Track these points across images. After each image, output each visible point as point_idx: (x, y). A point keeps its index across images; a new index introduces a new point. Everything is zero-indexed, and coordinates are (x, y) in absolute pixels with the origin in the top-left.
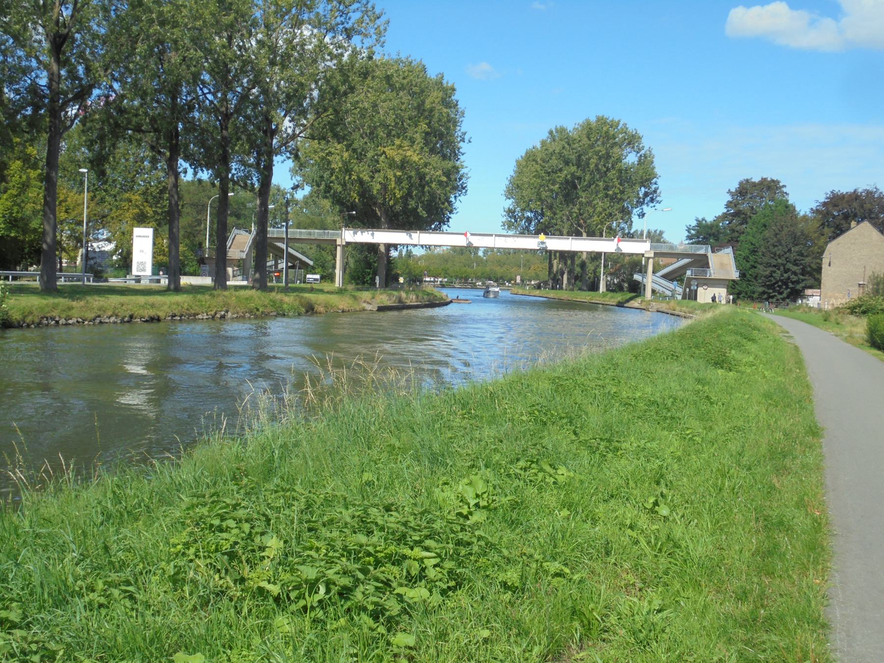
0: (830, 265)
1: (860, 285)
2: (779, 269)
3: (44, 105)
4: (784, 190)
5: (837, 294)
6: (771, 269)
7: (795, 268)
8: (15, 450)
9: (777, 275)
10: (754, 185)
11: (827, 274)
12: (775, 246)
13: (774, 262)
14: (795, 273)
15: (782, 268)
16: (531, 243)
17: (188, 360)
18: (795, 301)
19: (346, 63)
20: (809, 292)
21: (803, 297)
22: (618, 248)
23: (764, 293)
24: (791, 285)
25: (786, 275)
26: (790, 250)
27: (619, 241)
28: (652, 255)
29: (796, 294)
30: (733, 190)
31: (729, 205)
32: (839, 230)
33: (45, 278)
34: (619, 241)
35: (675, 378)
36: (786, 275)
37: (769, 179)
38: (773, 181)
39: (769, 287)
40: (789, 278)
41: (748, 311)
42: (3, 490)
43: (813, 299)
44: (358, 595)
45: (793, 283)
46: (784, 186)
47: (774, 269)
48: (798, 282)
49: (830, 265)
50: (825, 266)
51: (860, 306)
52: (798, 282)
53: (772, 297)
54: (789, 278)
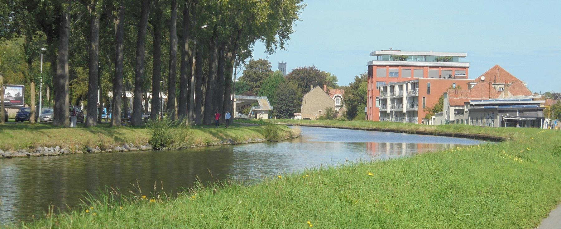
1: (319, 111)
2: (284, 105)
3: (123, 114)
4: (270, 65)
5: (308, 115)
6: (281, 105)
9: (284, 108)
11: (304, 107)
12: (282, 96)
13: (282, 102)
14: (291, 107)
15: (286, 105)
17: (372, 78)
18: (290, 118)
19: (50, 54)
20: (295, 114)
24: (289, 112)
25: (287, 108)
26: (288, 97)
29: (292, 115)
32: (306, 89)
35: (422, 177)
36: (287, 108)
37: (263, 60)
40: (288, 109)
41: (274, 120)
42: (195, 98)
43: (299, 117)
44: (196, 214)
45: (290, 111)
46: (270, 63)
47: (282, 105)
51: (340, 119)
53: (281, 117)
54: (288, 109)
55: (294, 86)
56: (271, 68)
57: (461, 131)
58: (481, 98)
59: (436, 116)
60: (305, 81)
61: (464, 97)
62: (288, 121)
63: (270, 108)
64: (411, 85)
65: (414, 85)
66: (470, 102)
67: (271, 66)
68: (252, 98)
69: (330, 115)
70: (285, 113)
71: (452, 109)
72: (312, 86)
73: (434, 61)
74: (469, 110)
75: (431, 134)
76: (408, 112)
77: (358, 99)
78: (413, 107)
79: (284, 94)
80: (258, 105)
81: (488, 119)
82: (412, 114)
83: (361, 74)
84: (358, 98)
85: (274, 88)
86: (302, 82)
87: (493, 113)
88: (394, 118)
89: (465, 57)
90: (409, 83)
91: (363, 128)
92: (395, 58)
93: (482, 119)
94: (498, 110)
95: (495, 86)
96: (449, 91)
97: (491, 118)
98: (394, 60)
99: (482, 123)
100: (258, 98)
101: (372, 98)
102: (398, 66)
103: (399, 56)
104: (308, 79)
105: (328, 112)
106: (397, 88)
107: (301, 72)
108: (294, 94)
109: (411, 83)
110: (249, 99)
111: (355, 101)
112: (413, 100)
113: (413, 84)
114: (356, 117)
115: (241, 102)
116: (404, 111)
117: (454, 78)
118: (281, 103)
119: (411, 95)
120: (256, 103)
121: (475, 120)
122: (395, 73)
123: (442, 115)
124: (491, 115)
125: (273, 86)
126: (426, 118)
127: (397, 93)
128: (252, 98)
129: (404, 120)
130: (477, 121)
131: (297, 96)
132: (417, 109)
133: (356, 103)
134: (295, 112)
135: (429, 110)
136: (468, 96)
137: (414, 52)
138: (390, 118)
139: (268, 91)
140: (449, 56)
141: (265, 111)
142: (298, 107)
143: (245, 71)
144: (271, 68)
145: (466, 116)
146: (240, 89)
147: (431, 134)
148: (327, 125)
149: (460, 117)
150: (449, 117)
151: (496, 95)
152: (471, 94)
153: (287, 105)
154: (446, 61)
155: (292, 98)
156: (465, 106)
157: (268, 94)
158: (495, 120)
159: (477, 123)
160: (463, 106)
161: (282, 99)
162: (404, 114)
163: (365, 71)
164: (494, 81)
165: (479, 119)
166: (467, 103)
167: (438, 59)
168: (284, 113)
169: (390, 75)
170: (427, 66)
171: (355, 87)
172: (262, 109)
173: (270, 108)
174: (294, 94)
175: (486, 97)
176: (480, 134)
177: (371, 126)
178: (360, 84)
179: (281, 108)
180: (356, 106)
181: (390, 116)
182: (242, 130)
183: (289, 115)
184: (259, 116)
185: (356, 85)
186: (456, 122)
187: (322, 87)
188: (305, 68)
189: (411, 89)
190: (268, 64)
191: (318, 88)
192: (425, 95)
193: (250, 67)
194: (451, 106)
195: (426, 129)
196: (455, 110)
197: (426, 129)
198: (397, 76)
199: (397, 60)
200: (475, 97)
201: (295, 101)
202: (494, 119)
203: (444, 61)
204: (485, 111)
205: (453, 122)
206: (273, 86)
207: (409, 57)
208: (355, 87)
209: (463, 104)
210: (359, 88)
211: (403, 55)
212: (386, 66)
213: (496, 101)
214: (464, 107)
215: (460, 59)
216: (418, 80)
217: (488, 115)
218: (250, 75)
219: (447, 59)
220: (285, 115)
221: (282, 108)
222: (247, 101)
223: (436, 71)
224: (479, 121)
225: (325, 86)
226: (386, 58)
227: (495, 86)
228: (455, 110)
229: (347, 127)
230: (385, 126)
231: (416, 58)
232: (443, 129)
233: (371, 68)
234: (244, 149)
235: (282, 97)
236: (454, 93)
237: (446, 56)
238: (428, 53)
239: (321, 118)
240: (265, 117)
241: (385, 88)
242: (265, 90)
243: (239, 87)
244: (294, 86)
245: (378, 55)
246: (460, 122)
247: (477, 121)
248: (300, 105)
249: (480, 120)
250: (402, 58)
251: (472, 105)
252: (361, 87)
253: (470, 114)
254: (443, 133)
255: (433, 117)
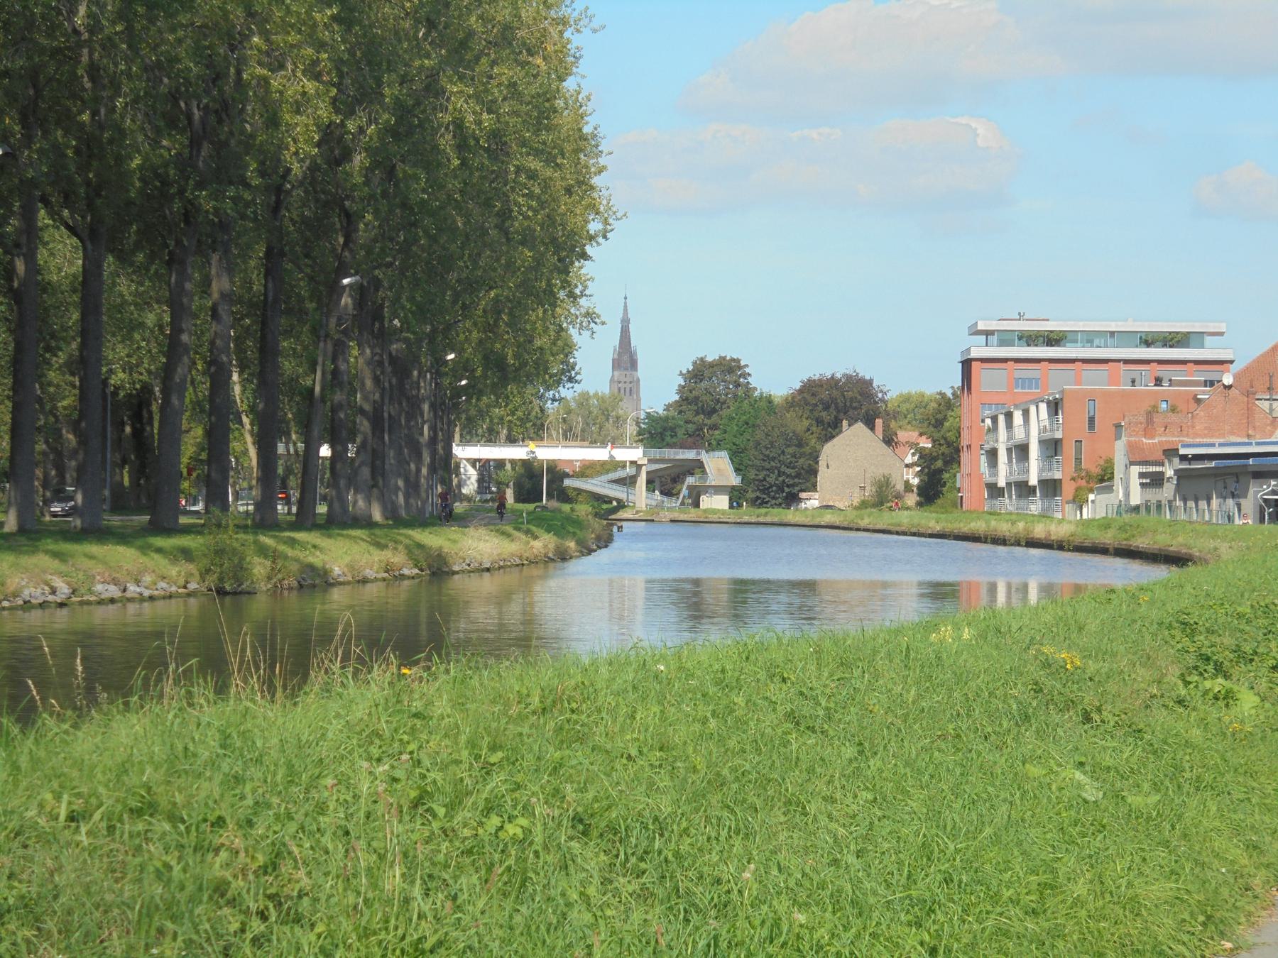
0: (828, 467)
2: (773, 473)
4: (747, 370)
7: (789, 471)
8: (29, 687)
9: (772, 479)
10: (712, 365)
12: (767, 448)
13: (766, 465)
14: (789, 476)
16: (546, 453)
20: (803, 495)
21: (800, 500)
22: (611, 456)
23: (758, 498)
24: (787, 490)
25: (781, 479)
27: (612, 448)
28: (646, 462)
29: (792, 499)
30: (684, 371)
31: (681, 389)
32: (830, 430)
33: (455, 481)
34: (612, 448)
36: (781, 479)
37: (728, 358)
38: (733, 360)
39: (763, 492)
43: (811, 502)
45: (788, 486)
46: (747, 366)
48: (793, 485)
49: (828, 467)
50: (822, 463)
52: (793, 485)
53: (767, 503)
55: (798, 424)
56: (750, 379)
57: (1133, 536)
58: (1224, 437)
59: (1098, 494)
60: (831, 410)
61: (1173, 435)
62: (766, 515)
63: (735, 480)
64: (1048, 407)
65: (1055, 407)
66: (1178, 450)
67: (749, 375)
68: (690, 455)
69: (883, 496)
70: (776, 492)
71: (1135, 470)
72: (845, 423)
73: (1137, 347)
74: (1176, 472)
75: (1060, 546)
76: (1043, 482)
77: (943, 454)
78: (1051, 470)
79: (771, 443)
80: (704, 472)
81: (1225, 498)
82: (1051, 487)
83: (952, 387)
84: (944, 449)
85: (750, 430)
86: (824, 414)
87: (1237, 482)
88: (1014, 501)
89: (1221, 334)
90: (1042, 401)
91: (914, 530)
92: (1030, 339)
93: (1209, 500)
94: (1250, 469)
95: (1271, 405)
96: (1127, 420)
97: (1233, 496)
98: (1029, 345)
99: (1197, 510)
100: (705, 457)
101: (969, 447)
102: (1038, 361)
103: (1042, 334)
104: (841, 405)
105: (880, 487)
106: (1018, 417)
107: (822, 386)
108: (800, 445)
109: (1049, 403)
110: (681, 457)
111: (935, 459)
112: (1052, 447)
113: (1053, 405)
114: (939, 501)
115: (662, 466)
116: (1033, 481)
117: (1170, 385)
118: (763, 468)
119: (1048, 435)
120: (698, 466)
121: (1191, 504)
122: (1030, 380)
123: (1110, 489)
124: (1232, 486)
125: (747, 424)
126: (1074, 501)
127: (1019, 434)
128: (690, 455)
129: (1033, 507)
130: (1185, 504)
131: (807, 450)
132: (1058, 476)
133: (939, 463)
134: (802, 491)
135: (1089, 477)
136: (1184, 432)
137: (1081, 323)
138: (1007, 501)
139: (735, 436)
140: (1177, 333)
141: (718, 490)
142: (808, 477)
143: (684, 387)
144: (750, 379)
145: (1168, 491)
146: (668, 433)
147: (1060, 546)
148: (846, 524)
149: (1154, 495)
150: (1127, 494)
151: (1269, 428)
152: (1193, 427)
153: (779, 472)
154: (1171, 347)
155: (794, 456)
156: (1166, 461)
157: (734, 444)
158: (1242, 501)
159: (1185, 509)
160: (1163, 465)
161: (768, 456)
162: (1032, 490)
163: (955, 379)
164: (1269, 388)
165: (1202, 500)
166: (1171, 453)
167: (1148, 341)
168: (772, 494)
169: (1017, 387)
170: (1118, 361)
171: (937, 420)
172: (713, 484)
173: (735, 480)
174: (800, 445)
175: (1238, 436)
176: (1171, 549)
177: (932, 524)
178: (950, 413)
179: (765, 479)
180: (940, 471)
181: (1038, 495)
182: (56, 555)
183: (786, 498)
184: (707, 502)
185: (939, 417)
186: (1143, 510)
187: (872, 427)
188: (833, 377)
189: (1046, 417)
190: (740, 368)
191: (860, 426)
192: (1083, 432)
193: (695, 376)
194: (1132, 463)
195: (1049, 533)
196: (1142, 475)
197: (1049, 532)
198: (1037, 388)
199: (1036, 345)
200: (1206, 436)
201: (802, 460)
202: (1239, 497)
203: (1165, 346)
204: (1216, 475)
205: (1136, 509)
206: (747, 424)
207: (1070, 336)
208: (937, 420)
209: (1159, 455)
210: (947, 424)
211: (1051, 332)
212: (1005, 360)
213: (1221, 445)
214: (1163, 465)
215: (1208, 339)
216: (1062, 392)
217: (1225, 488)
218: (697, 398)
219: (1172, 339)
220: (776, 499)
221: (768, 479)
222: (678, 463)
223: (1148, 372)
224: (1203, 504)
225: (879, 422)
226: (1006, 338)
227: (1271, 405)
228: (1142, 475)
229: (884, 527)
230: (962, 525)
231: (1090, 338)
232: (1090, 532)
233: (967, 364)
234: (97, 621)
235: (768, 452)
236: (1141, 423)
237: (1170, 333)
238: (1120, 323)
239: (864, 505)
240: (721, 502)
241: (995, 419)
242: (726, 436)
243: (665, 429)
244: (798, 424)
245: (988, 333)
246: (1153, 509)
247: (1185, 504)
248: (814, 472)
249: (1205, 502)
250: (1053, 339)
251: (1184, 458)
252: (951, 419)
253: (1178, 485)
254: (1087, 543)
255: (1091, 497)
